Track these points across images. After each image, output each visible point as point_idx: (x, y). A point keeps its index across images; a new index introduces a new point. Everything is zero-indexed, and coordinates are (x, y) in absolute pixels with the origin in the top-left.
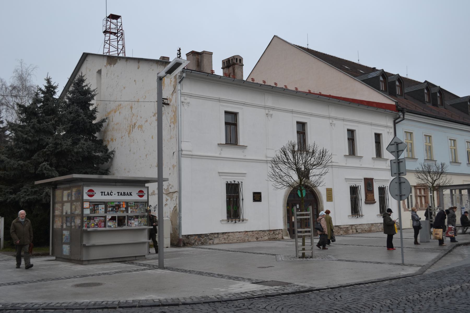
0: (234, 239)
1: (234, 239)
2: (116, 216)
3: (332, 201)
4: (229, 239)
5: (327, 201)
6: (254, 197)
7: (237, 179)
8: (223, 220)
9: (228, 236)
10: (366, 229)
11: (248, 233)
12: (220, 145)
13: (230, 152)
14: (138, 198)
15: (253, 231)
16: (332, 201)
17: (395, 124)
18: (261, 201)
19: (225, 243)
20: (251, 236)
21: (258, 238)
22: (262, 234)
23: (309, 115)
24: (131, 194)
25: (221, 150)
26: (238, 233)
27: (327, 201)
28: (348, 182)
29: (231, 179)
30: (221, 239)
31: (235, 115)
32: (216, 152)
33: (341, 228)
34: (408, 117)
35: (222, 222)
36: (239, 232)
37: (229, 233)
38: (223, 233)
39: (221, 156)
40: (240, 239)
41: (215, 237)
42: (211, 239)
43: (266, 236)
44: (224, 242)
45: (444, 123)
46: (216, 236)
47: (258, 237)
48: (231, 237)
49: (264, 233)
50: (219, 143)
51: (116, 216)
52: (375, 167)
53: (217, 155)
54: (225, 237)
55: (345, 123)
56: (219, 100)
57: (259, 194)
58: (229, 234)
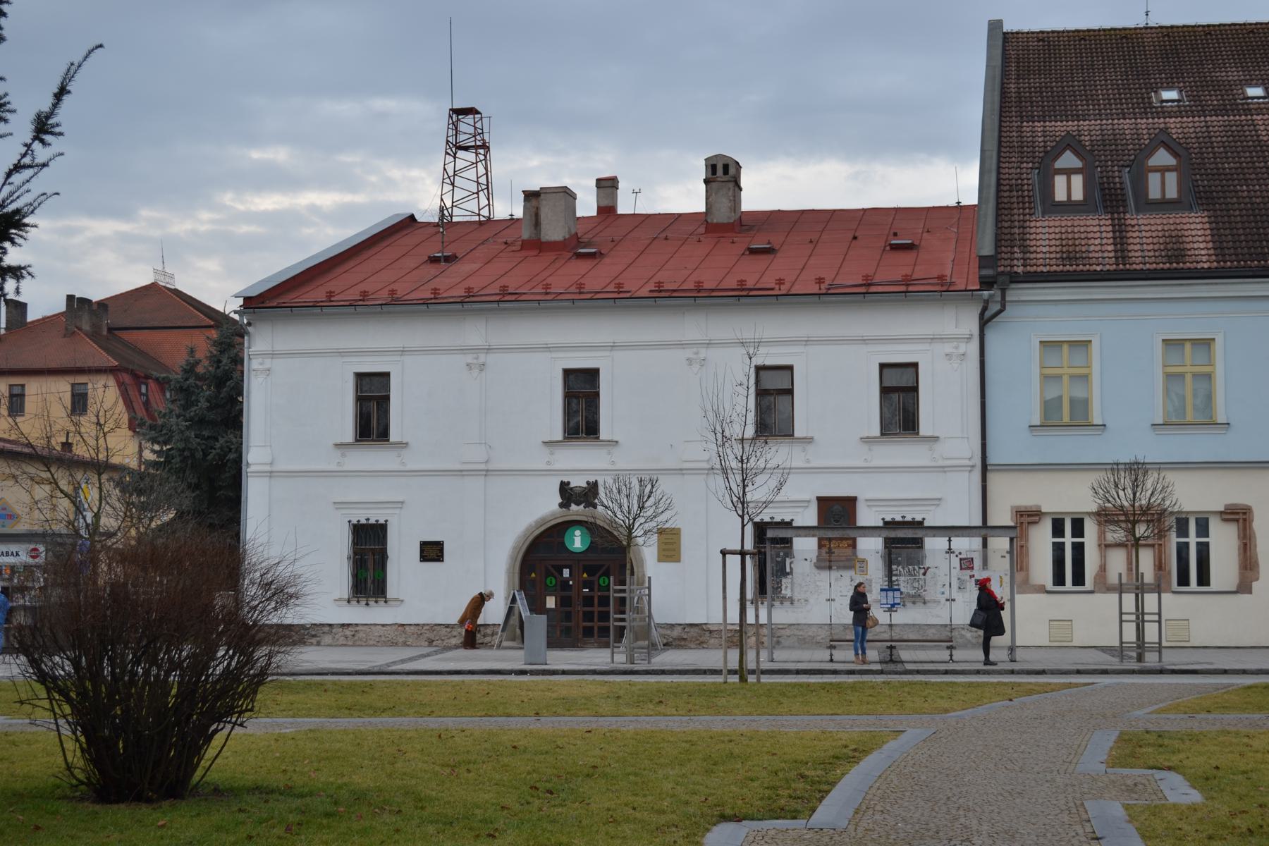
0: (370, 639)
1: (370, 639)
2: (1178, 543)
3: (678, 560)
4: (356, 638)
5: (660, 560)
6: (422, 551)
7: (375, 516)
8: (340, 599)
9: (356, 631)
10: (819, 638)
11: (407, 628)
12: (339, 446)
13: (372, 458)
14: (30, 561)
15: (418, 625)
16: (678, 560)
17: (984, 322)
18: (443, 561)
19: (345, 645)
20: (413, 634)
21: (433, 641)
22: (444, 631)
23: (925, 341)
24: (17, 554)
25: (552, 454)
26: (380, 627)
27: (660, 560)
28: (874, 509)
29: (361, 516)
30: (337, 637)
31: (592, 375)
32: (330, 462)
33: (711, 632)
34: (1059, 294)
35: (337, 603)
36: (383, 625)
37: (357, 625)
38: (343, 625)
39: (340, 469)
40: (383, 639)
41: (324, 633)
42: (314, 636)
43: (455, 637)
44: (344, 643)
45: (1239, 287)
46: (326, 629)
47: (433, 638)
48: (361, 635)
49: (448, 630)
50: (338, 442)
51: (1178, 543)
52: (875, 463)
53: (333, 467)
54: (348, 632)
55: (554, 355)
56: (340, 353)
57: (424, 545)
58: (358, 628)
